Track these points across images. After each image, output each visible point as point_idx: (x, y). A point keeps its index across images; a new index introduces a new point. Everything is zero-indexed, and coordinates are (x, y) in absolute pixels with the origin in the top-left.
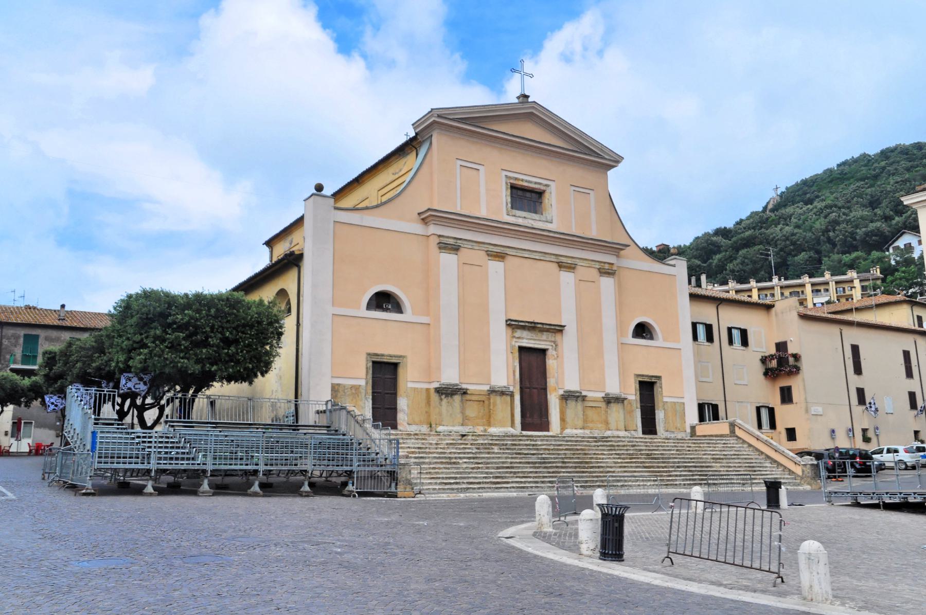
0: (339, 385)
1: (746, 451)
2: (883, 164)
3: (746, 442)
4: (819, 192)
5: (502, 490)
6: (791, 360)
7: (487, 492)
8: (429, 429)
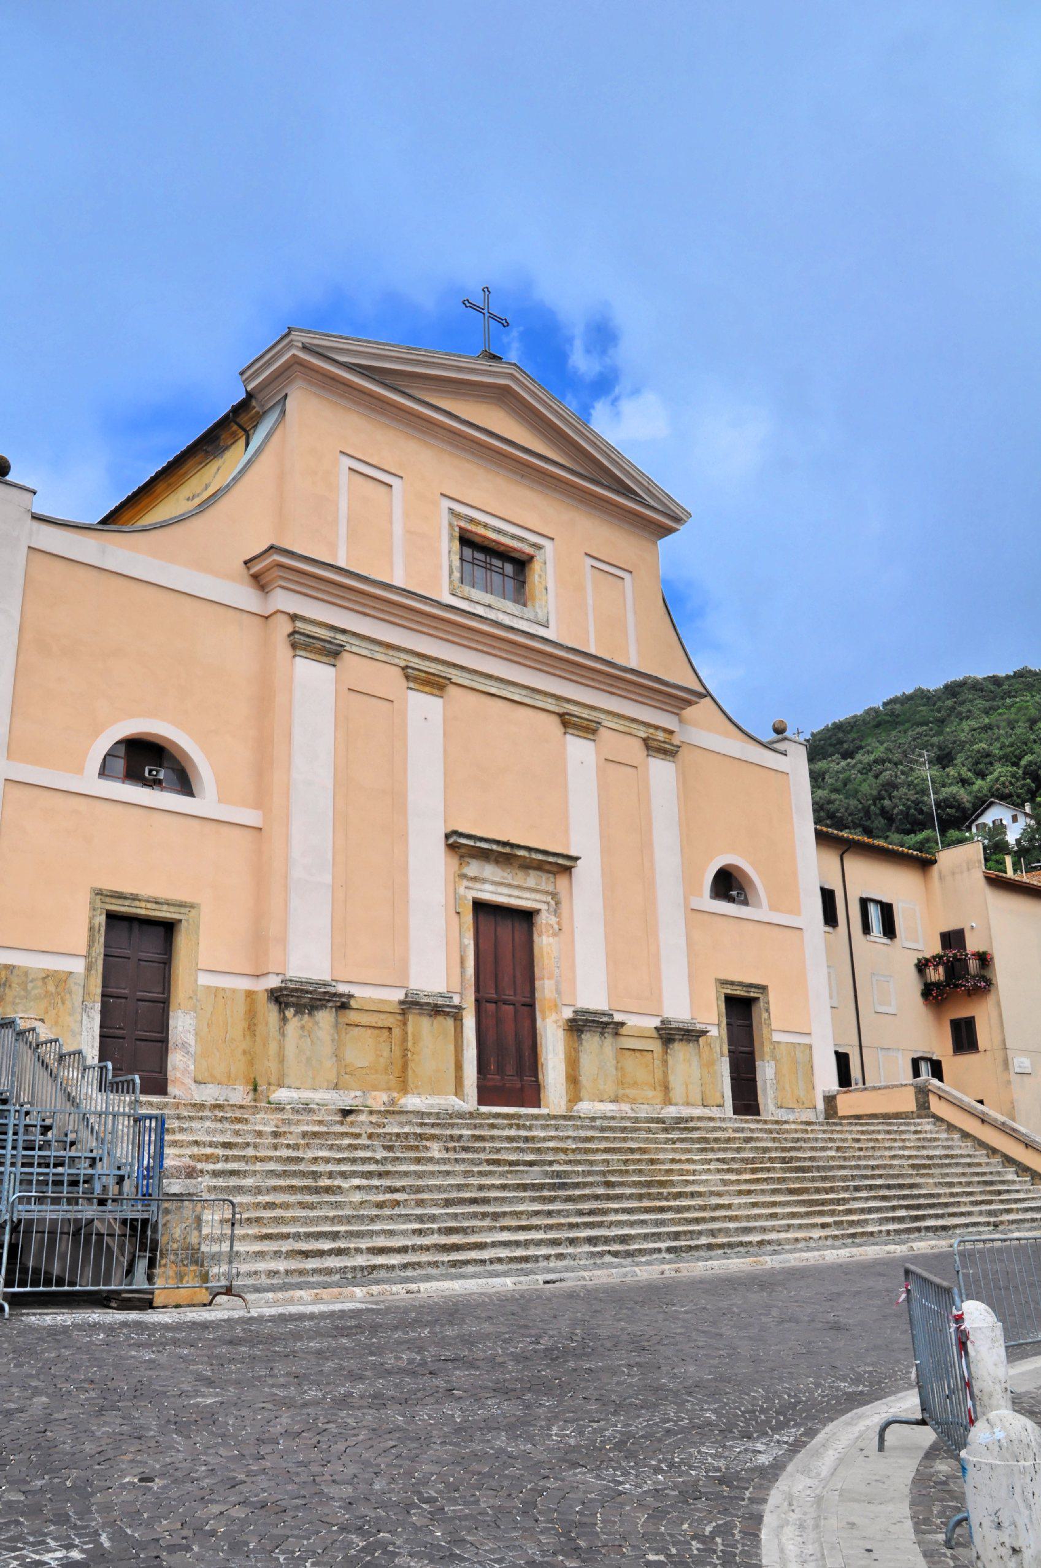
1: (964, 1148)
2: (949, 703)
3: (956, 1127)
4: (861, 741)
5: (470, 1269)
6: (973, 964)
7: (428, 1278)
8: (251, 1095)
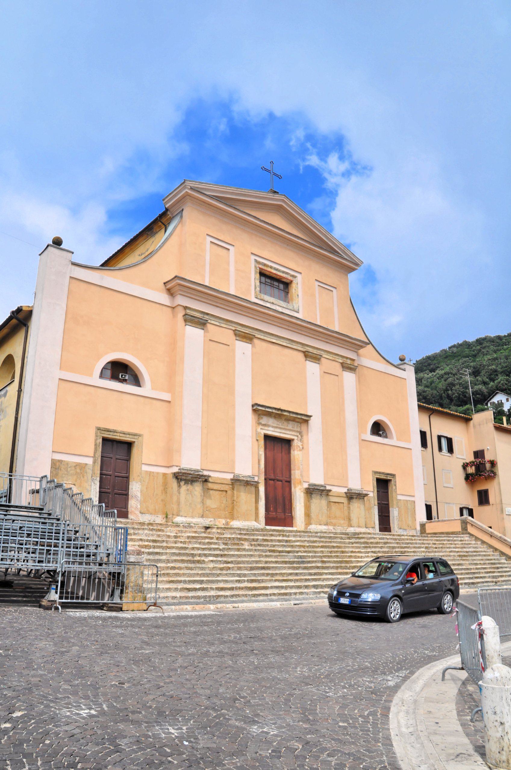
0: (60, 461)
2: (478, 347)
3: (479, 539)
5: (261, 598)
